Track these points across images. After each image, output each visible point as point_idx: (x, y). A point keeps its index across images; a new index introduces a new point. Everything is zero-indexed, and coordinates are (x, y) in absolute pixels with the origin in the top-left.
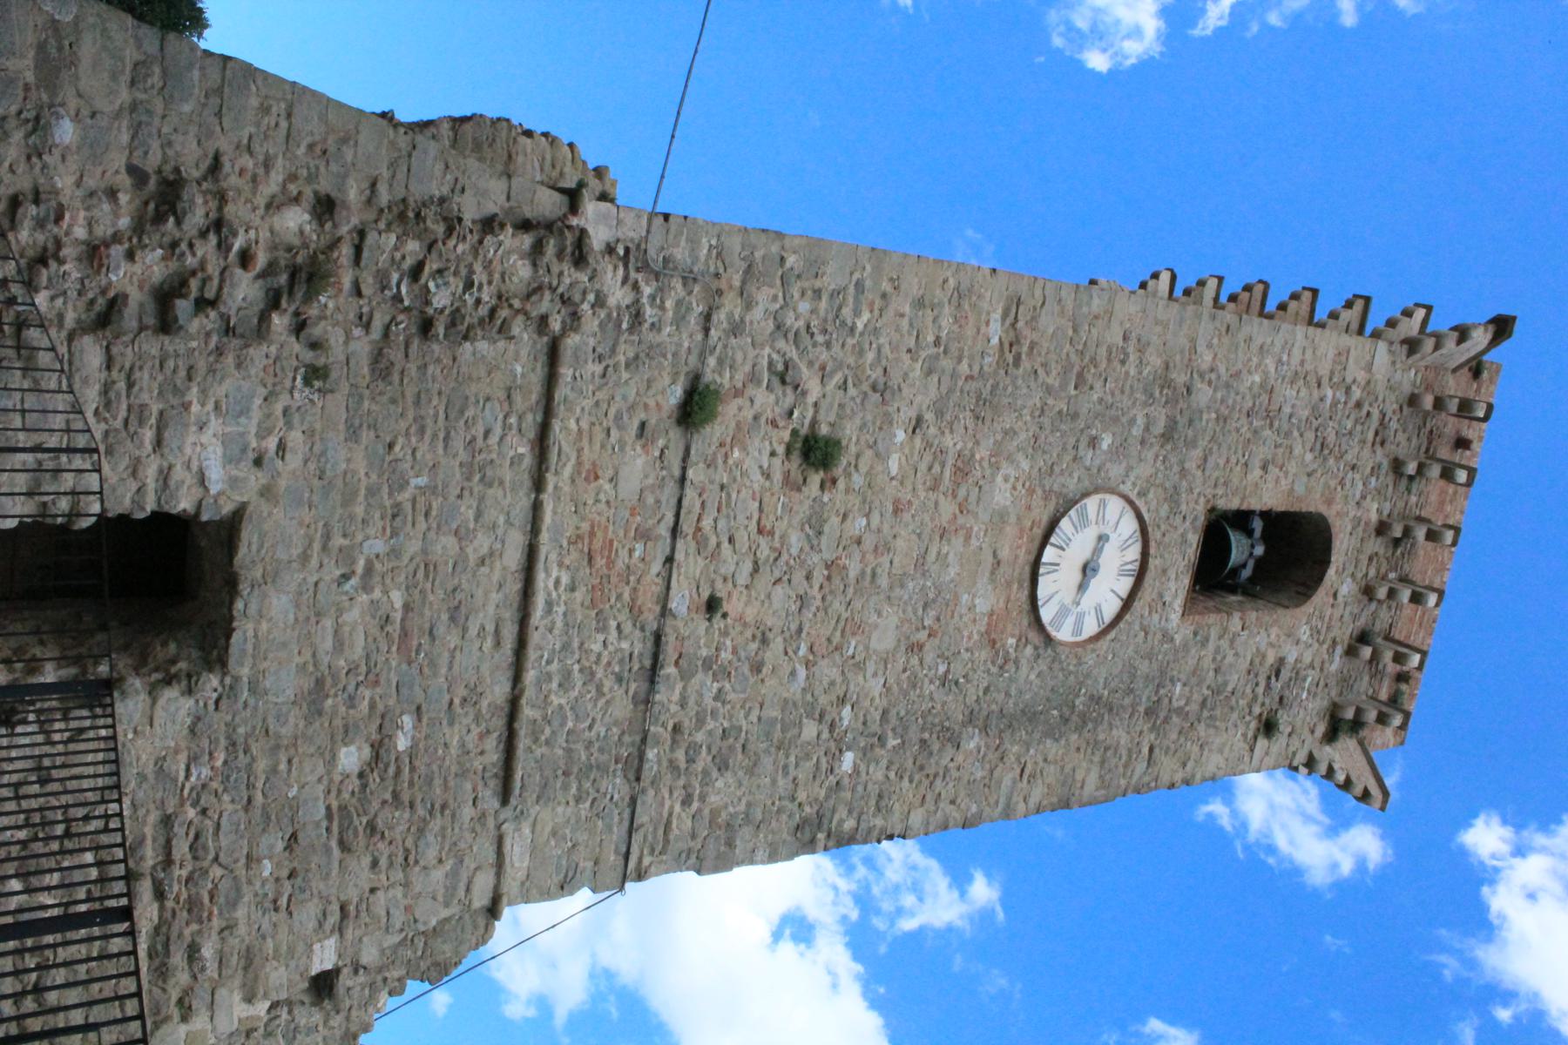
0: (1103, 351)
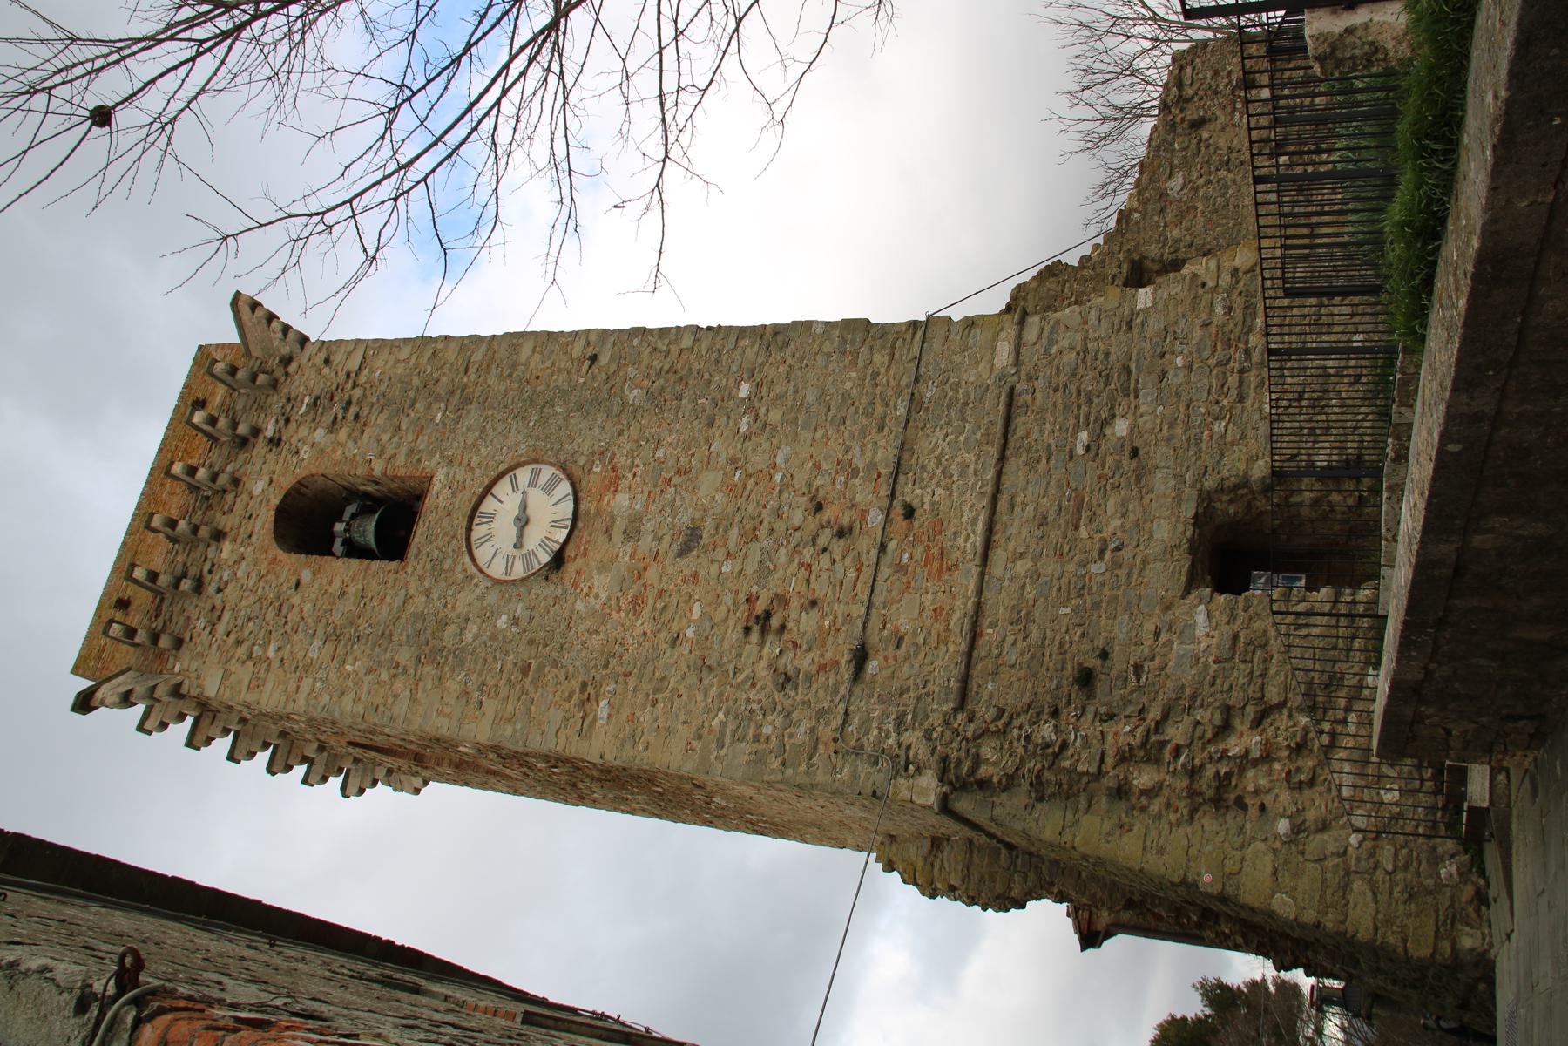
0: (503, 692)
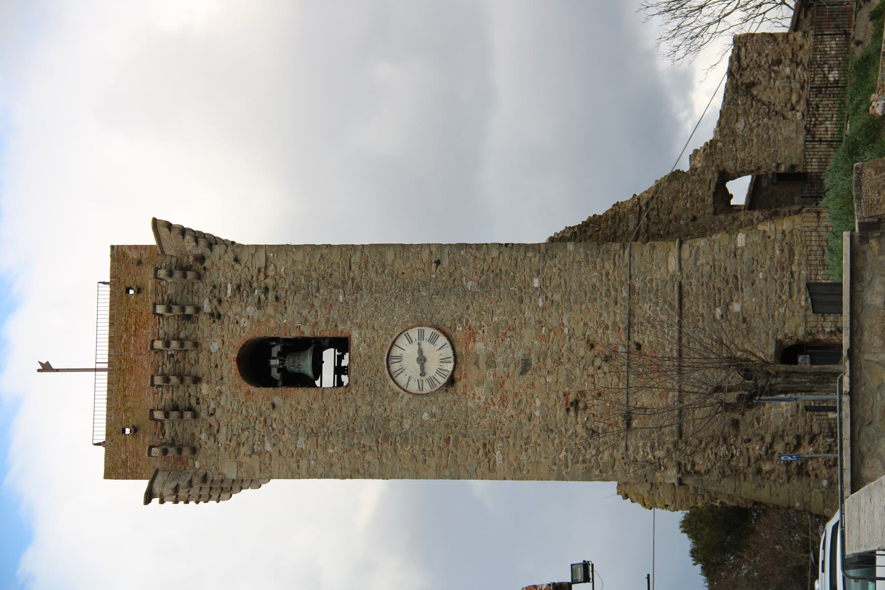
0: (437, 453)
